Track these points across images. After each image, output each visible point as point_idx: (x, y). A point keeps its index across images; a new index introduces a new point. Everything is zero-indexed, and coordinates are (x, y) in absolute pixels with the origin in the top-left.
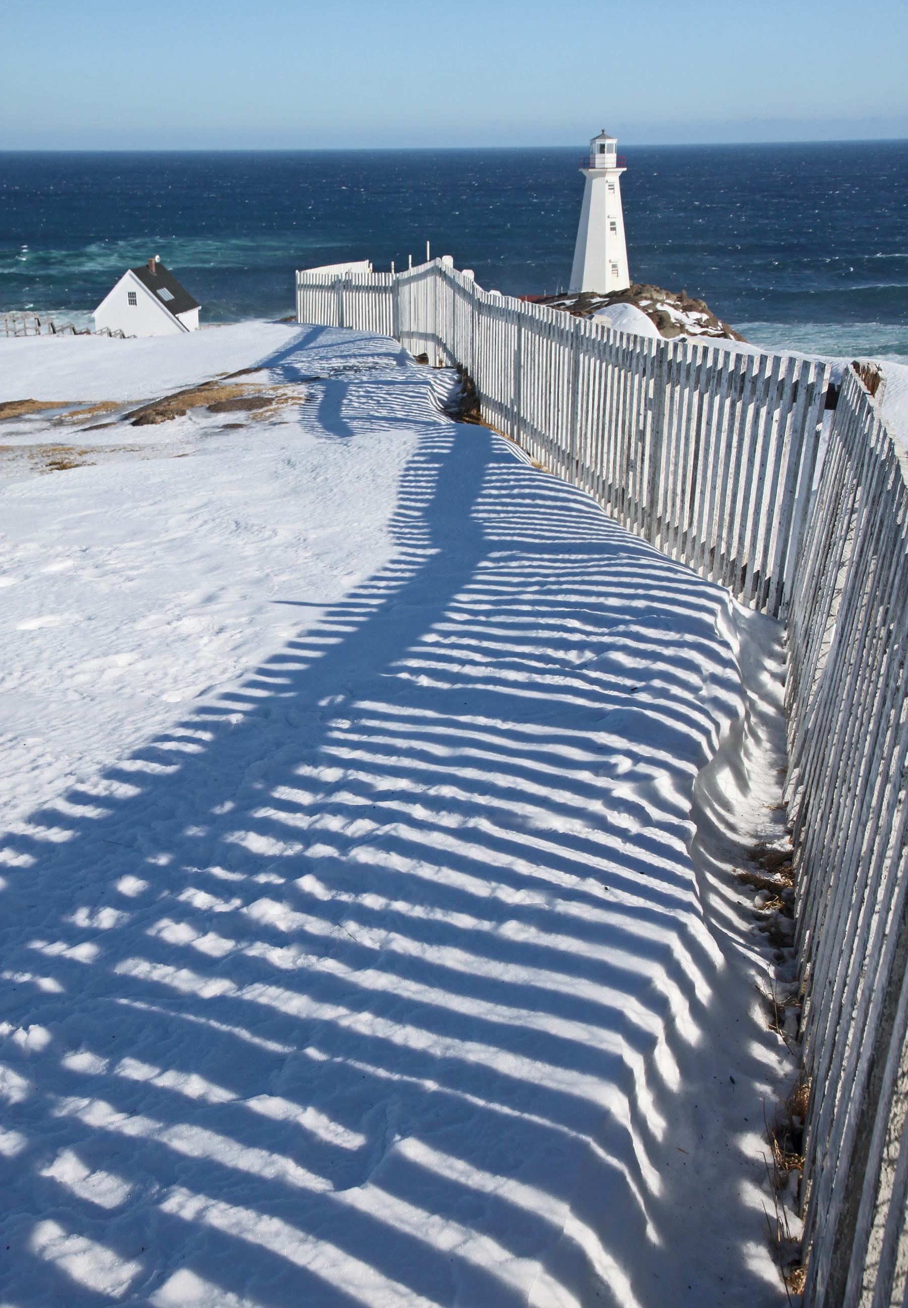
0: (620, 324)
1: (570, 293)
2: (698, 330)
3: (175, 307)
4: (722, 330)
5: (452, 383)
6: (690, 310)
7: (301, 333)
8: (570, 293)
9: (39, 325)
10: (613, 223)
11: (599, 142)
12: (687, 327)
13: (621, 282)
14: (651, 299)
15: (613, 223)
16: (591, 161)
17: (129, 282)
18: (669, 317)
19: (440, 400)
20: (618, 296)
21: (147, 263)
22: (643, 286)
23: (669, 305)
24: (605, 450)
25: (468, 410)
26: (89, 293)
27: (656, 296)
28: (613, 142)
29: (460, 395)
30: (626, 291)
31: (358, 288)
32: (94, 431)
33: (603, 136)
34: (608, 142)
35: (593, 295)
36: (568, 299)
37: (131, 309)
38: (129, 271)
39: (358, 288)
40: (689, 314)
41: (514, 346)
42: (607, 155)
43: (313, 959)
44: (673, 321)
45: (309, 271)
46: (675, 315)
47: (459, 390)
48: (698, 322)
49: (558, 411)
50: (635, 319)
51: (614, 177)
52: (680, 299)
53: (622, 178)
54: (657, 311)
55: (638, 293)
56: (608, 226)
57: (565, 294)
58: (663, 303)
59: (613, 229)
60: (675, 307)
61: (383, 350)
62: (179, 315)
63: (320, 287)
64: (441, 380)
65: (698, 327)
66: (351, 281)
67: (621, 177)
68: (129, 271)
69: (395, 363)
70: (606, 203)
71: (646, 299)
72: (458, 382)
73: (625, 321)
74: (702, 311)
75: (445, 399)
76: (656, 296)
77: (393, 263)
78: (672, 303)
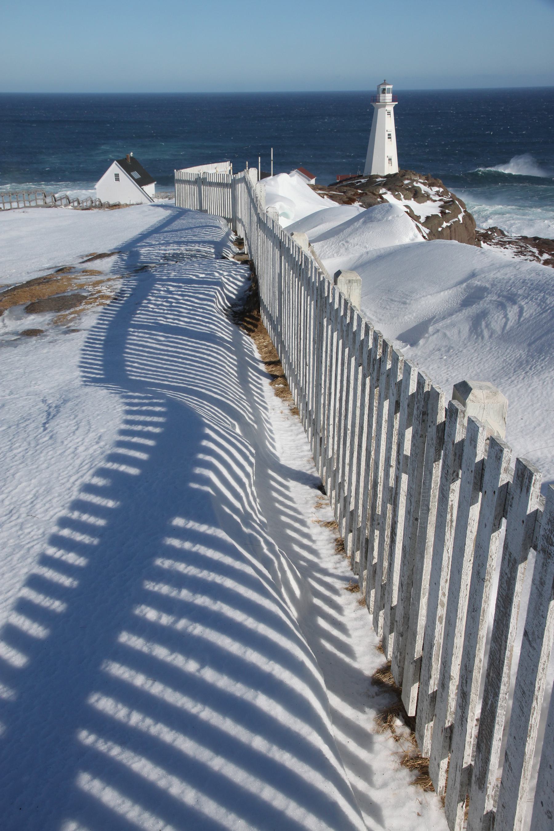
0: (386, 220)
1: (364, 175)
2: (438, 198)
3: (141, 182)
5: (243, 280)
6: (433, 186)
7: (171, 215)
9: (45, 197)
10: (389, 135)
11: (382, 87)
12: (431, 196)
14: (410, 179)
15: (389, 135)
16: (378, 98)
17: (115, 168)
19: (229, 298)
20: (392, 177)
21: (125, 157)
22: (406, 171)
23: (421, 183)
24: (347, 461)
25: (250, 311)
26: (93, 175)
27: (413, 177)
28: (390, 87)
29: (248, 292)
30: (396, 174)
31: (211, 184)
32: (100, 252)
33: (385, 83)
34: (388, 87)
35: (377, 176)
36: (363, 179)
37: (115, 184)
38: (115, 162)
39: (211, 184)
40: (433, 188)
41: (277, 271)
42: (387, 95)
43: (149, 721)
44: (423, 192)
45: (183, 171)
46: (424, 189)
47: (247, 287)
48: (437, 193)
49: (306, 365)
50: (398, 216)
51: (390, 108)
52: (427, 179)
53: (395, 108)
54: (414, 187)
55: (403, 176)
56: (387, 136)
57: (362, 176)
59: (389, 138)
60: (424, 184)
61: (209, 238)
62: (144, 187)
63: (188, 182)
66: (206, 178)
67: (394, 108)
68: (115, 162)
69: (213, 251)
70: (386, 123)
71: (408, 179)
72: (249, 279)
73: (390, 218)
74: (439, 187)
75: (234, 297)
76: (413, 177)
77: (247, 163)
78: (422, 181)
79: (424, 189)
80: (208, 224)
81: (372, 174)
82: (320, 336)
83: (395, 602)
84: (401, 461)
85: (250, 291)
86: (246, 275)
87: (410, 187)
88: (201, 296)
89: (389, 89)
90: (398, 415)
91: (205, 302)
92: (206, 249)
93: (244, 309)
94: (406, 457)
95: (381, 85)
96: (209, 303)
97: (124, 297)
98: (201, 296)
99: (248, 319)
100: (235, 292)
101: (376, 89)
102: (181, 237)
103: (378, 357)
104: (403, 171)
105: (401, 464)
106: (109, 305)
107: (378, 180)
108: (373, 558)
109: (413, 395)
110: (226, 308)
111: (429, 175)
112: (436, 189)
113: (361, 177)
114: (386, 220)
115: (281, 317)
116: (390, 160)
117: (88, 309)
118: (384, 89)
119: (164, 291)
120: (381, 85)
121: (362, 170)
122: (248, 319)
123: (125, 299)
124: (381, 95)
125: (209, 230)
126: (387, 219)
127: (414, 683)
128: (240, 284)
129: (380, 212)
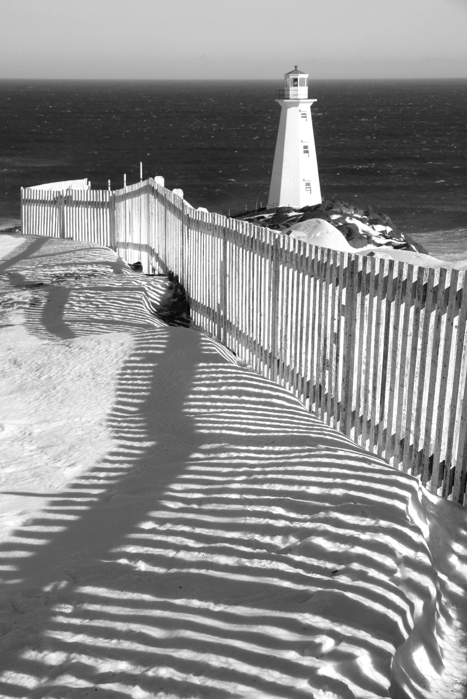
0: (314, 237)
1: (268, 207)
2: (383, 241)
4: (404, 241)
5: (164, 289)
6: (376, 224)
8: (268, 207)
10: (306, 147)
11: (292, 76)
12: (374, 238)
13: (315, 198)
14: (341, 213)
15: (306, 147)
16: (286, 93)
18: (357, 229)
19: (154, 304)
24: (304, 350)
25: (179, 313)
27: (345, 211)
28: (306, 76)
31: (78, 204)
33: (296, 71)
34: (300, 76)
35: (289, 209)
36: (267, 213)
39: (78, 204)
40: (375, 226)
41: (220, 257)
44: (361, 233)
45: (33, 188)
46: (362, 227)
47: (170, 295)
48: (383, 234)
50: (327, 232)
51: (306, 106)
52: (367, 213)
54: (346, 224)
55: (329, 208)
57: (264, 209)
58: (351, 217)
59: (307, 152)
60: (363, 221)
63: (43, 202)
64: (154, 287)
65: (383, 238)
66: (71, 197)
67: (312, 107)
70: (298, 131)
71: (336, 213)
72: (170, 288)
73: (318, 234)
74: (386, 225)
75: (158, 304)
76: (345, 211)
78: (360, 217)
79: (362, 227)
80: (92, 246)
81: (280, 206)
82: (276, 280)
83: (340, 400)
84: (341, 310)
85: (174, 298)
86: (167, 284)
87: (340, 224)
88: (127, 299)
89: (303, 79)
90: (338, 287)
91: (133, 304)
92: (103, 269)
93: (172, 313)
94: (343, 306)
95: (290, 73)
96: (138, 305)
97: (42, 303)
98: (127, 299)
99: (178, 322)
100: (159, 300)
101: (282, 77)
102: (64, 260)
103: (325, 262)
104: (328, 202)
105: (341, 312)
106: (28, 309)
107: (290, 215)
108: (325, 390)
109: (346, 268)
110: (153, 312)
111: (370, 208)
112: (380, 228)
113: (263, 210)
114: (314, 237)
115: (225, 303)
116: (308, 184)
117: (9, 312)
118: (296, 80)
119: (83, 297)
120: (290, 73)
121: (266, 199)
122: (178, 322)
123: (43, 304)
124: (292, 88)
125: (98, 252)
126: (314, 236)
127: (352, 427)
128: (162, 293)
129: (306, 228)
